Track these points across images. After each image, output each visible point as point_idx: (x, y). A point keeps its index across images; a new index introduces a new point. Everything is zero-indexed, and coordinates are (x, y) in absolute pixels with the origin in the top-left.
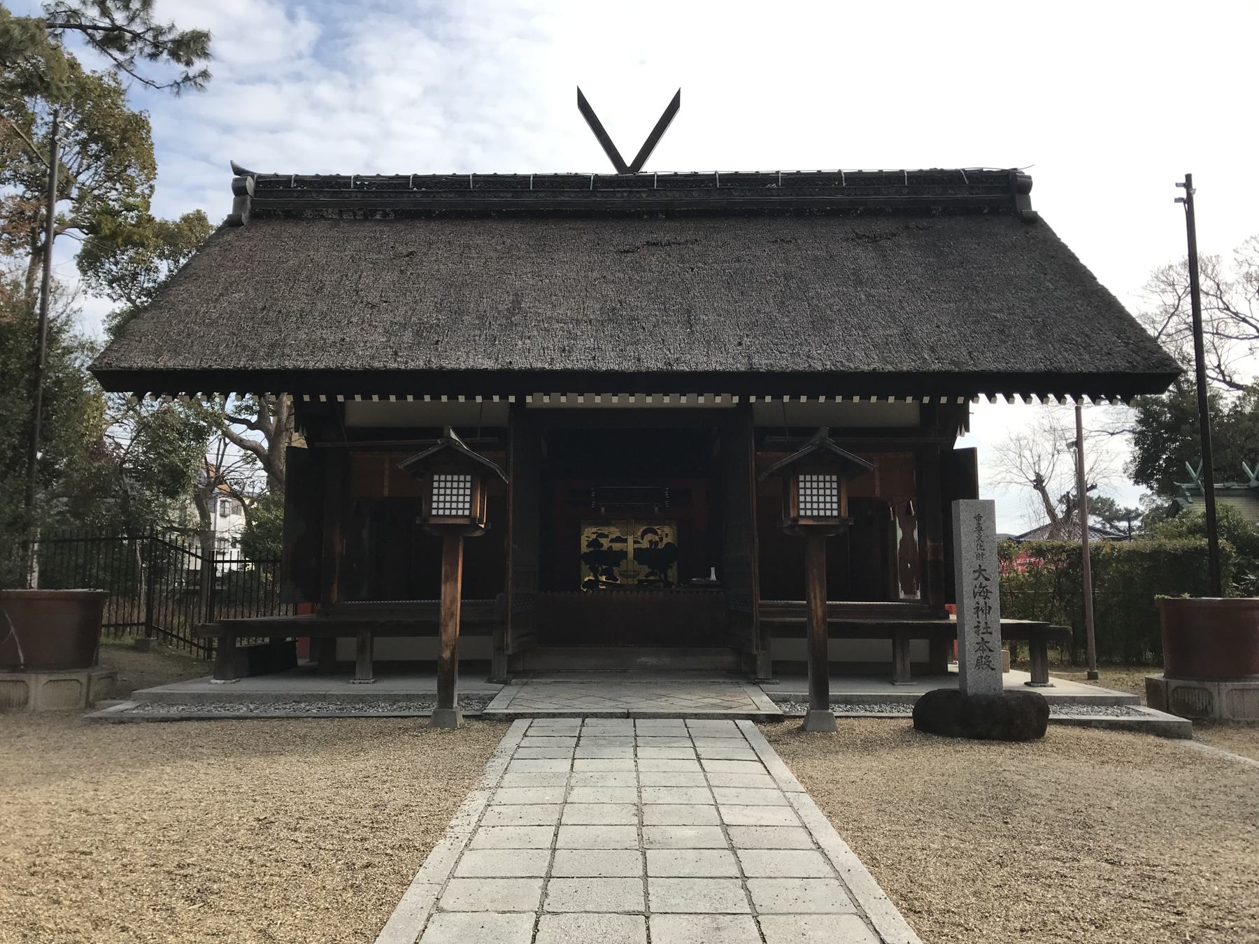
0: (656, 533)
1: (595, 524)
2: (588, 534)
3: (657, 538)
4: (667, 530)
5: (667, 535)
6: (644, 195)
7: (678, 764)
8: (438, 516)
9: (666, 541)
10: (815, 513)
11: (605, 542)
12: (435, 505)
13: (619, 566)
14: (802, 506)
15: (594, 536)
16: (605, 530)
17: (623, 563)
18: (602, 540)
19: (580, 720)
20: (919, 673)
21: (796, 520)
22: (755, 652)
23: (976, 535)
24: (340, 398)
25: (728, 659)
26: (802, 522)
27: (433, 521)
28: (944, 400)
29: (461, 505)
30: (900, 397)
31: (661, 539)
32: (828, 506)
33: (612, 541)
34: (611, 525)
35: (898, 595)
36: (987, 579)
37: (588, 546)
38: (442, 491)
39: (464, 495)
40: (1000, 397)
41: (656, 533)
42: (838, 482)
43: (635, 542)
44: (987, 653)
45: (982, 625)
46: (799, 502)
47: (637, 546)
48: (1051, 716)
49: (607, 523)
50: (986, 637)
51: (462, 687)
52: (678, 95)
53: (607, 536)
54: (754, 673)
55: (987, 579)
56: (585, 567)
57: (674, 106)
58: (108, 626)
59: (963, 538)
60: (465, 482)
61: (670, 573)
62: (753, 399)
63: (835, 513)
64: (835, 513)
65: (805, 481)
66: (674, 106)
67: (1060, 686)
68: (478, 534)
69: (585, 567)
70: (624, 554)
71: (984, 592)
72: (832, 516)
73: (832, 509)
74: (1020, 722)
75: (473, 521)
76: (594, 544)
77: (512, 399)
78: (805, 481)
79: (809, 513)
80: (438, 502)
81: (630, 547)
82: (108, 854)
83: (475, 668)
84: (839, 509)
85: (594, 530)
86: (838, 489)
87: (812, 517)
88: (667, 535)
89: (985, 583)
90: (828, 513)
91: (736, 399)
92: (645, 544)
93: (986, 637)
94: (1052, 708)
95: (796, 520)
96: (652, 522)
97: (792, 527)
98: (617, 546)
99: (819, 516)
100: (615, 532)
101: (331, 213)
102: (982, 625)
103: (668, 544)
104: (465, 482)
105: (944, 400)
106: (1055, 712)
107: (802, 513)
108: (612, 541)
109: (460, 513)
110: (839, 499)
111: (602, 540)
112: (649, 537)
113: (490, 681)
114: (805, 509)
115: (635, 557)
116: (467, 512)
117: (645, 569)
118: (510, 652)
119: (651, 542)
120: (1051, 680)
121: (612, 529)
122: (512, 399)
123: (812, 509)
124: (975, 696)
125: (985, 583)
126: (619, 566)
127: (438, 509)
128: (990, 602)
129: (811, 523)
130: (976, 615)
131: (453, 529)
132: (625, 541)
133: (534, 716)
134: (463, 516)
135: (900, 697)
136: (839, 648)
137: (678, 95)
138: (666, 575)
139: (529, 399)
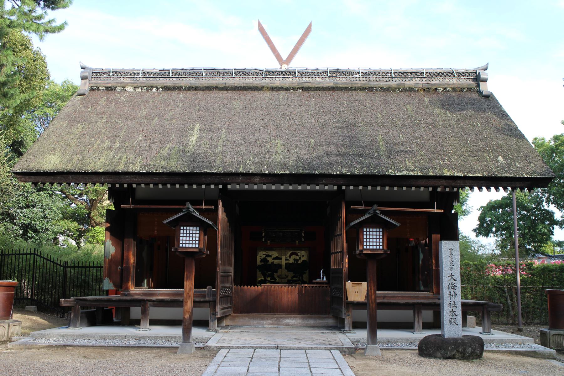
0: (297, 255)
1: (265, 249)
2: (261, 255)
3: (298, 258)
4: (303, 253)
5: (303, 256)
7: (299, 370)
8: (182, 247)
9: (302, 259)
10: (371, 247)
11: (270, 260)
12: (181, 242)
13: (277, 272)
14: (365, 244)
15: (264, 256)
16: (270, 253)
17: (279, 271)
18: (269, 259)
19: (253, 350)
20: (426, 326)
21: (361, 251)
22: (344, 317)
23: (450, 258)
25: (331, 321)
26: (364, 252)
29: (194, 242)
31: (300, 258)
32: (378, 244)
33: (274, 259)
34: (274, 250)
35: (419, 287)
36: (455, 280)
37: (261, 261)
38: (185, 235)
39: (196, 234)
40: (476, 188)
41: (297, 255)
42: (383, 232)
43: (286, 260)
44: (455, 317)
45: (452, 303)
46: (363, 242)
47: (287, 262)
49: (271, 249)
50: (454, 309)
51: (196, 332)
52: (310, 26)
53: (271, 256)
54: (344, 327)
55: (455, 280)
56: (259, 273)
57: (308, 30)
59: (444, 260)
60: (379, 232)
61: (304, 276)
62: (344, 188)
63: (381, 247)
64: (381, 247)
65: (366, 231)
66: (308, 30)
67: (497, 335)
68: (204, 256)
69: (259, 273)
70: (280, 266)
71: (454, 287)
72: (379, 249)
73: (379, 246)
74: (470, 350)
75: (200, 251)
76: (264, 260)
77: (220, 187)
78: (366, 231)
79: (368, 247)
80: (183, 240)
81: (283, 262)
82: (497, 123)
83: (203, 324)
84: (383, 246)
85: (264, 253)
86: (383, 235)
87: (370, 250)
88: (303, 256)
89: (454, 282)
90: (378, 247)
92: (291, 261)
95: (361, 251)
96: (295, 249)
97: (360, 254)
98: (276, 262)
99: (373, 249)
100: (275, 254)
101: (213, 324)
102: (452, 303)
103: (304, 261)
107: (365, 247)
108: (274, 259)
109: (194, 246)
110: (383, 240)
111: (269, 259)
112: (294, 257)
113: (208, 330)
114: (367, 245)
115: (286, 268)
116: (197, 246)
117: (291, 274)
118: (219, 316)
119: (294, 259)
121: (274, 252)
122: (220, 187)
123: (370, 245)
124: (447, 339)
125: (454, 282)
126: (277, 272)
127: (183, 244)
128: (456, 292)
129: (369, 252)
130: (452, 298)
131: (189, 254)
132: (281, 259)
133: (230, 348)
134: (195, 248)
136: (383, 315)
137: (310, 26)
138: (302, 278)
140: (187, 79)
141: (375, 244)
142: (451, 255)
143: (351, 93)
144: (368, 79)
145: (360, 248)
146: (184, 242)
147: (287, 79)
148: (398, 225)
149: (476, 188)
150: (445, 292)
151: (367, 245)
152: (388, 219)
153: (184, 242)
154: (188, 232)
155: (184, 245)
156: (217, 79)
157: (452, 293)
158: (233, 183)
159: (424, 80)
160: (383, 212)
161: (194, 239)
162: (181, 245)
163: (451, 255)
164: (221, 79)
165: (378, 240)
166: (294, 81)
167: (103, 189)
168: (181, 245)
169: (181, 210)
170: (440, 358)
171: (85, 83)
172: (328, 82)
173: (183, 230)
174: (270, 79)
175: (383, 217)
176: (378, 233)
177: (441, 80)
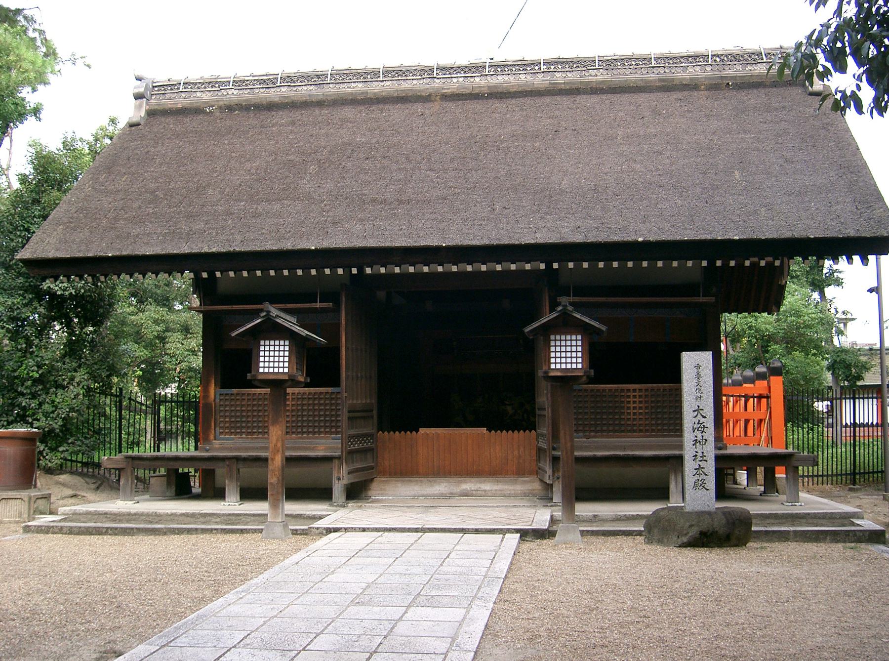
6: (477, 79)
8: (264, 373)
10: (563, 366)
21: (546, 372)
24: (556, 266)
27: (260, 377)
28: (719, 263)
30: (333, 268)
32: (574, 360)
36: (704, 417)
40: (856, 258)
44: (703, 476)
45: (700, 454)
48: (754, 528)
50: (703, 464)
55: (704, 417)
58: (803, 476)
60: (576, 340)
79: (558, 366)
87: (561, 370)
90: (574, 366)
91: (368, 271)
93: (703, 464)
94: (754, 521)
95: (546, 372)
102: (700, 454)
104: (576, 340)
105: (719, 263)
106: (757, 525)
120: (803, 495)
122: (704, 263)
128: (706, 436)
129: (559, 374)
134: (283, 373)
135: (809, 514)
139: (542, 266)
140: (305, 88)
141: (271, 364)
142: (698, 376)
143: (578, 98)
144: (610, 72)
145: (545, 368)
146: (267, 364)
147: (472, 80)
148: (604, 328)
149: (856, 258)
150: (688, 436)
151: (556, 363)
152: (587, 321)
153: (267, 364)
154: (277, 348)
155: (266, 370)
156: (354, 85)
157: (699, 438)
158: (418, 263)
159: (708, 68)
160: (577, 306)
161: (574, 354)
162: (261, 370)
163: (698, 376)
164: (360, 85)
165: (281, 359)
166: (483, 82)
167: (182, 281)
168: (261, 370)
169: (256, 313)
170: (138, 475)
171: (140, 106)
172: (540, 81)
173: (555, 340)
174: (443, 80)
175: (578, 316)
176: (282, 348)
177: (739, 67)
